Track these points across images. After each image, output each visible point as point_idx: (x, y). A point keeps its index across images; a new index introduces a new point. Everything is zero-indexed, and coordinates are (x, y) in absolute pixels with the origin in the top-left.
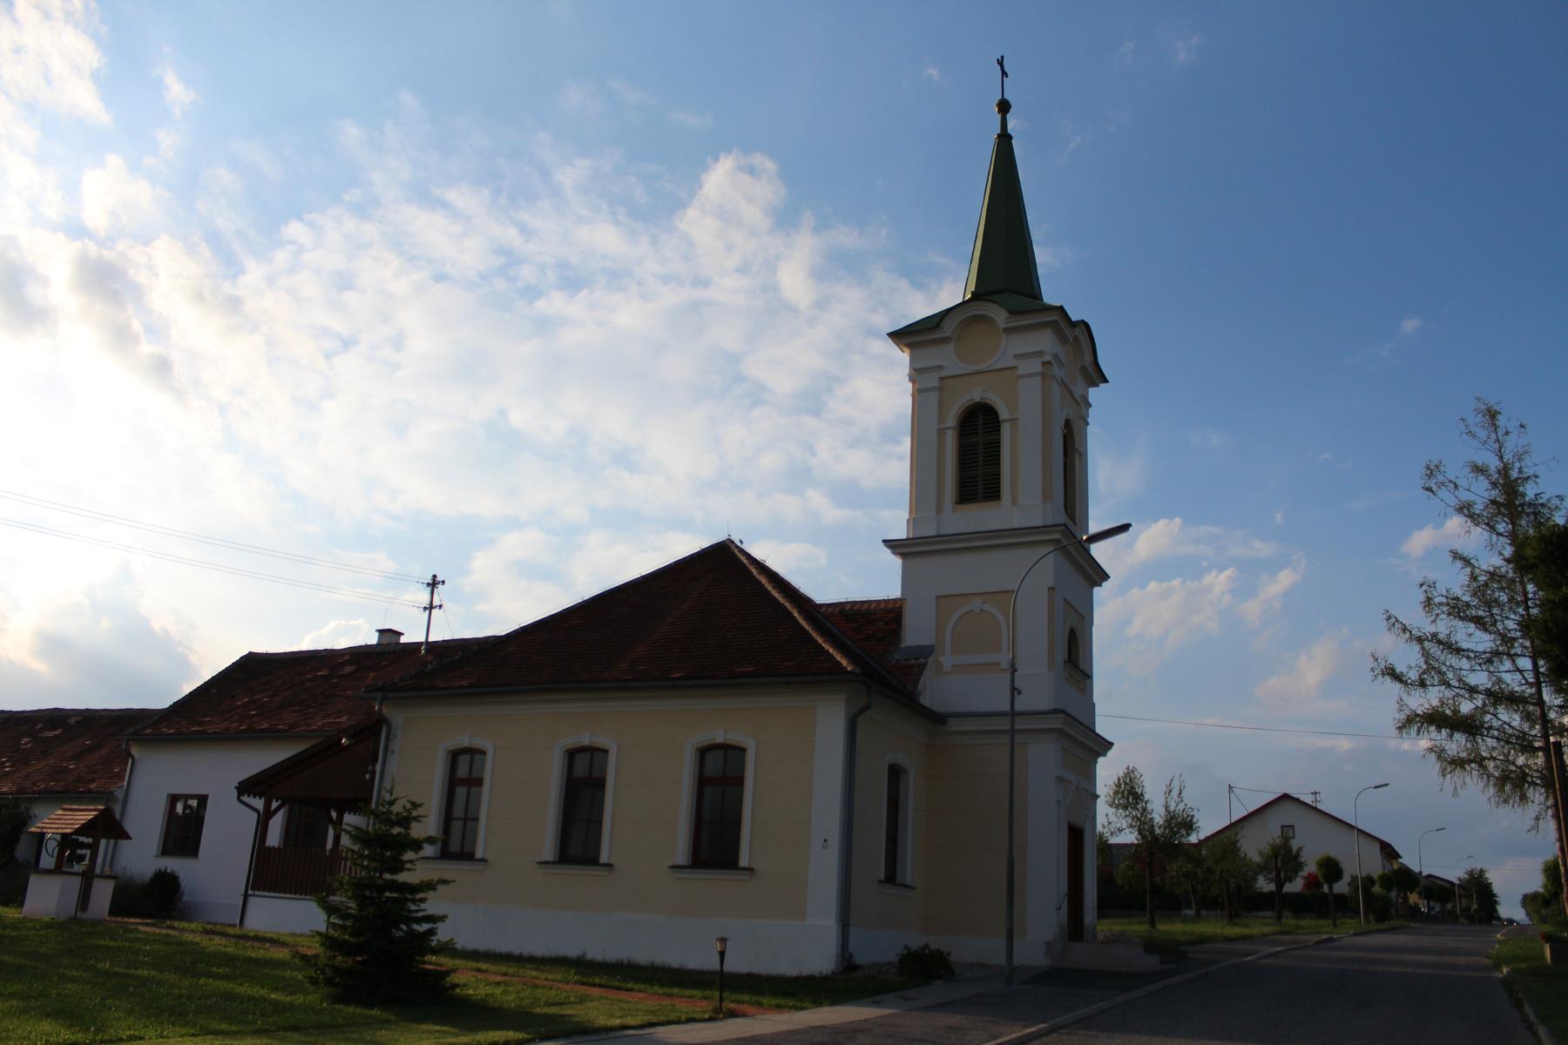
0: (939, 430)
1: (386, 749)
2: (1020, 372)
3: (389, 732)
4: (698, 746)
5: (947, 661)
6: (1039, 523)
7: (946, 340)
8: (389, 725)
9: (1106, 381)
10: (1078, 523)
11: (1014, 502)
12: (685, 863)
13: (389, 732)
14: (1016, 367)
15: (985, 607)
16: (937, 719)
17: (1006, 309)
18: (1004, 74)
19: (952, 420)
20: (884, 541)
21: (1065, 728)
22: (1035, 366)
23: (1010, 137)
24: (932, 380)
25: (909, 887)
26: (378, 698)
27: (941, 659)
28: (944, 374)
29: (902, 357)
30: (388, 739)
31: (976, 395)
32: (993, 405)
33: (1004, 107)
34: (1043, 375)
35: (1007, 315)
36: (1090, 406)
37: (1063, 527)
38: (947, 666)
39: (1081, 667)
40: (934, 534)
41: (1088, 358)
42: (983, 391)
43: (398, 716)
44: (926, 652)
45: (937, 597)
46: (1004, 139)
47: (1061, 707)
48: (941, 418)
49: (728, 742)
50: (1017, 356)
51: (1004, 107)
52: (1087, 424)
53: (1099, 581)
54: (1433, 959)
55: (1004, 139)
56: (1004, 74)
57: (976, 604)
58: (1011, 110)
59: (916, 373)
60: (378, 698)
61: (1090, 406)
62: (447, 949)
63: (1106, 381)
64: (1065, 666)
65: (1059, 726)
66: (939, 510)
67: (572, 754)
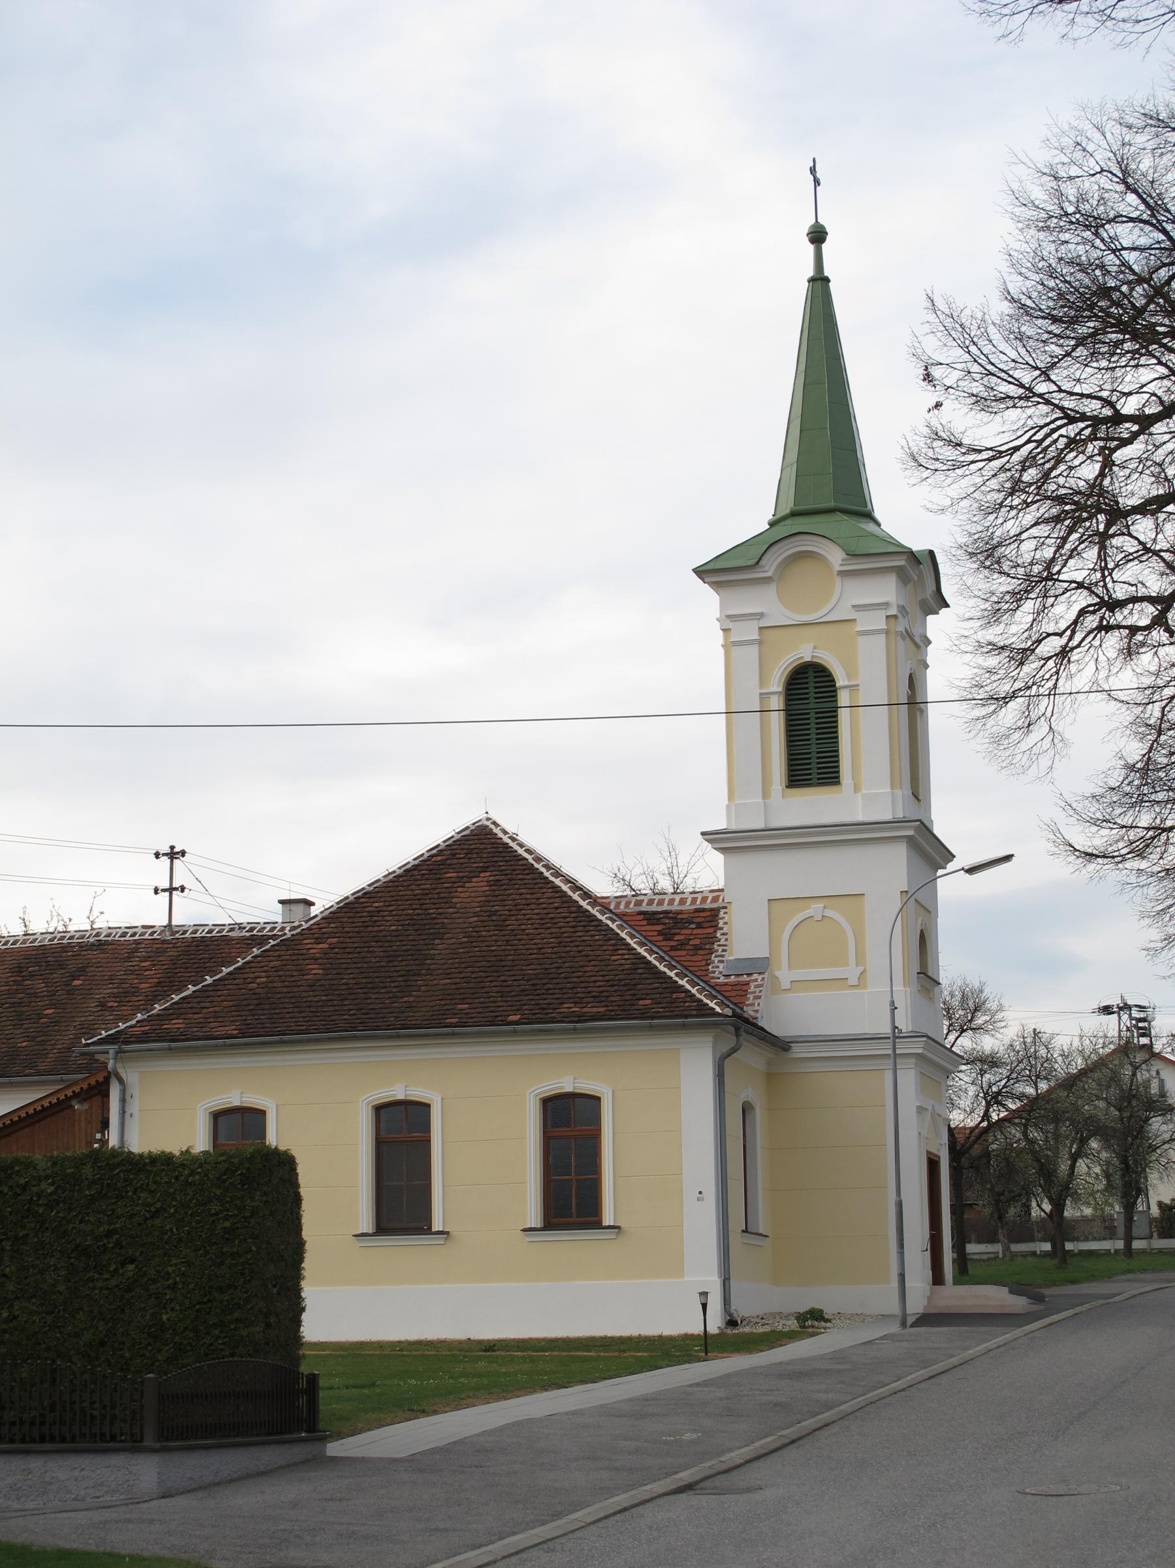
0: (761, 694)
1: (123, 1112)
2: (859, 628)
3: (123, 1092)
4: (541, 1096)
5: (784, 974)
6: (888, 817)
7: (767, 580)
8: (121, 1081)
9: (947, 606)
10: (920, 798)
11: (857, 789)
12: (539, 1226)
13: (123, 1092)
14: (855, 620)
15: (828, 913)
16: (781, 1045)
17: (844, 550)
18: (817, 182)
19: (776, 684)
20: (703, 834)
21: (927, 1053)
22: (877, 621)
23: (827, 280)
24: (749, 631)
25: (761, 1235)
26: (111, 1052)
27: (777, 973)
28: (764, 623)
29: (708, 599)
30: (123, 1101)
31: (806, 653)
32: (828, 667)
33: (818, 236)
34: (887, 632)
35: (844, 555)
36: (930, 642)
37: (919, 823)
38: (785, 984)
39: (930, 974)
40: (761, 825)
41: (931, 587)
42: (815, 648)
43: (132, 1074)
44: (760, 966)
45: (769, 900)
46: (819, 282)
47: (924, 1030)
48: (763, 679)
49: (577, 1091)
50: (857, 608)
51: (818, 236)
52: (927, 666)
53: (943, 864)
54: (584, 1051)
55: (819, 282)
56: (817, 182)
57: (815, 909)
58: (828, 237)
59: (729, 621)
60: (111, 1052)
61: (930, 642)
62: (969, 1254)
63: (947, 606)
64: (918, 978)
65: (920, 1051)
66: (766, 794)
67: (381, 1110)
